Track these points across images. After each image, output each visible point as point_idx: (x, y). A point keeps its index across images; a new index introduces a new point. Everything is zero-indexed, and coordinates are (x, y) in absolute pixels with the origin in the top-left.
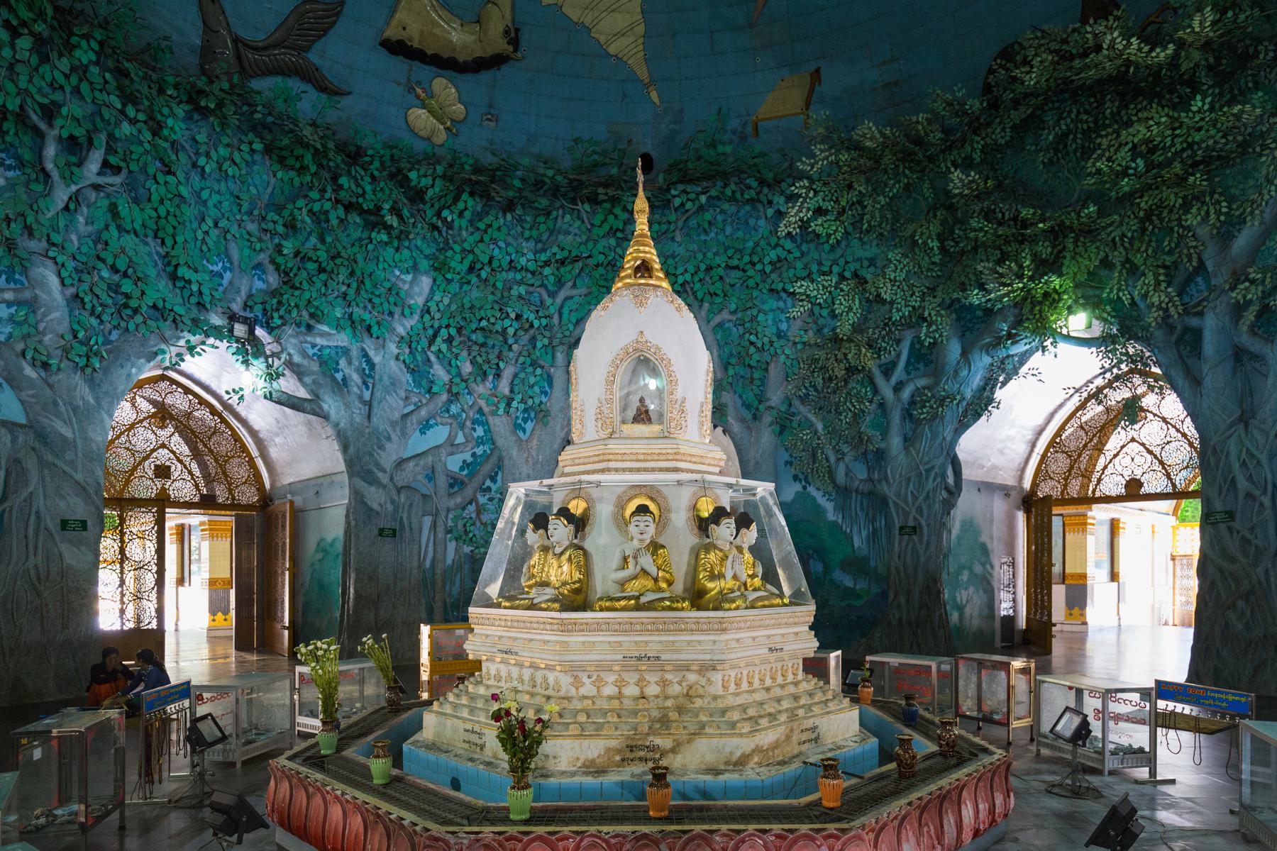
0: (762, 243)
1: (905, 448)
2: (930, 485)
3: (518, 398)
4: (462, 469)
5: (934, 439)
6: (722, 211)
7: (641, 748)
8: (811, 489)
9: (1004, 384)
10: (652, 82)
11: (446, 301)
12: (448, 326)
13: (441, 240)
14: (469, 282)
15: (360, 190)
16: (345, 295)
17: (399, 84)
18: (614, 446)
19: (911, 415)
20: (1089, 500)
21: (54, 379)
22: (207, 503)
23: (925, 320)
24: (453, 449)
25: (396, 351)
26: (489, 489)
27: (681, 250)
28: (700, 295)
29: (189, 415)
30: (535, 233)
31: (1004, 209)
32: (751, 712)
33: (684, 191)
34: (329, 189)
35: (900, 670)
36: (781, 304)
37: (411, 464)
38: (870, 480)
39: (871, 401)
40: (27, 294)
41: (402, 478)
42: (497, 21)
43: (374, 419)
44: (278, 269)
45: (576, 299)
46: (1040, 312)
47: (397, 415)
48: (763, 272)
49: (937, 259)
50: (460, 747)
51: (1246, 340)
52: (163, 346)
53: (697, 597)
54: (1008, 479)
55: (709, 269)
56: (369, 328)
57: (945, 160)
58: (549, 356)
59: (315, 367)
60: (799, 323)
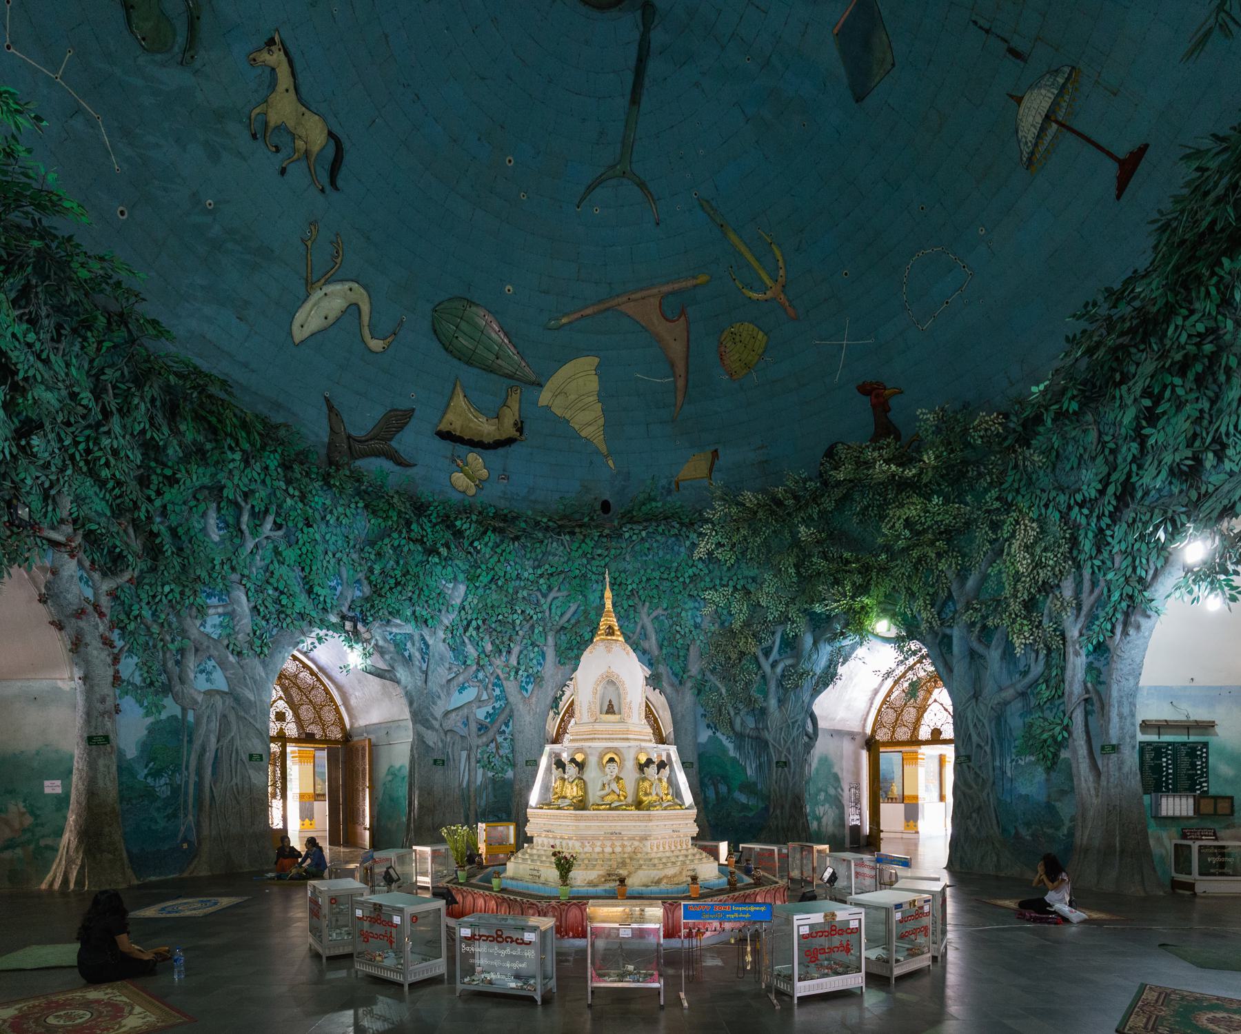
1: (779, 707)
2: (795, 733)
3: (523, 668)
4: (486, 718)
5: (797, 701)
6: (657, 541)
7: (613, 875)
8: (718, 734)
9: (843, 663)
10: (610, 454)
11: (476, 601)
12: (477, 619)
13: (472, 560)
14: (490, 588)
15: (425, 533)
18: (598, 727)
19: (782, 685)
20: (915, 742)
21: (243, 662)
22: (306, 738)
23: (789, 619)
24: (481, 704)
25: (443, 636)
26: (504, 732)
27: (630, 567)
29: (296, 676)
30: (533, 555)
31: (833, 551)
32: (664, 860)
33: (631, 529)
34: (404, 531)
35: (761, 853)
36: (697, 605)
37: (454, 714)
38: (757, 729)
39: (756, 674)
40: (229, 609)
41: (449, 724)
42: (510, 417)
43: (429, 684)
44: (370, 583)
45: (561, 599)
46: (859, 618)
47: (444, 681)
48: (684, 583)
49: (795, 580)
51: (975, 645)
52: (303, 638)
53: (639, 805)
54: (855, 726)
56: (426, 622)
57: (796, 517)
58: (543, 639)
59: (392, 648)
60: (709, 618)
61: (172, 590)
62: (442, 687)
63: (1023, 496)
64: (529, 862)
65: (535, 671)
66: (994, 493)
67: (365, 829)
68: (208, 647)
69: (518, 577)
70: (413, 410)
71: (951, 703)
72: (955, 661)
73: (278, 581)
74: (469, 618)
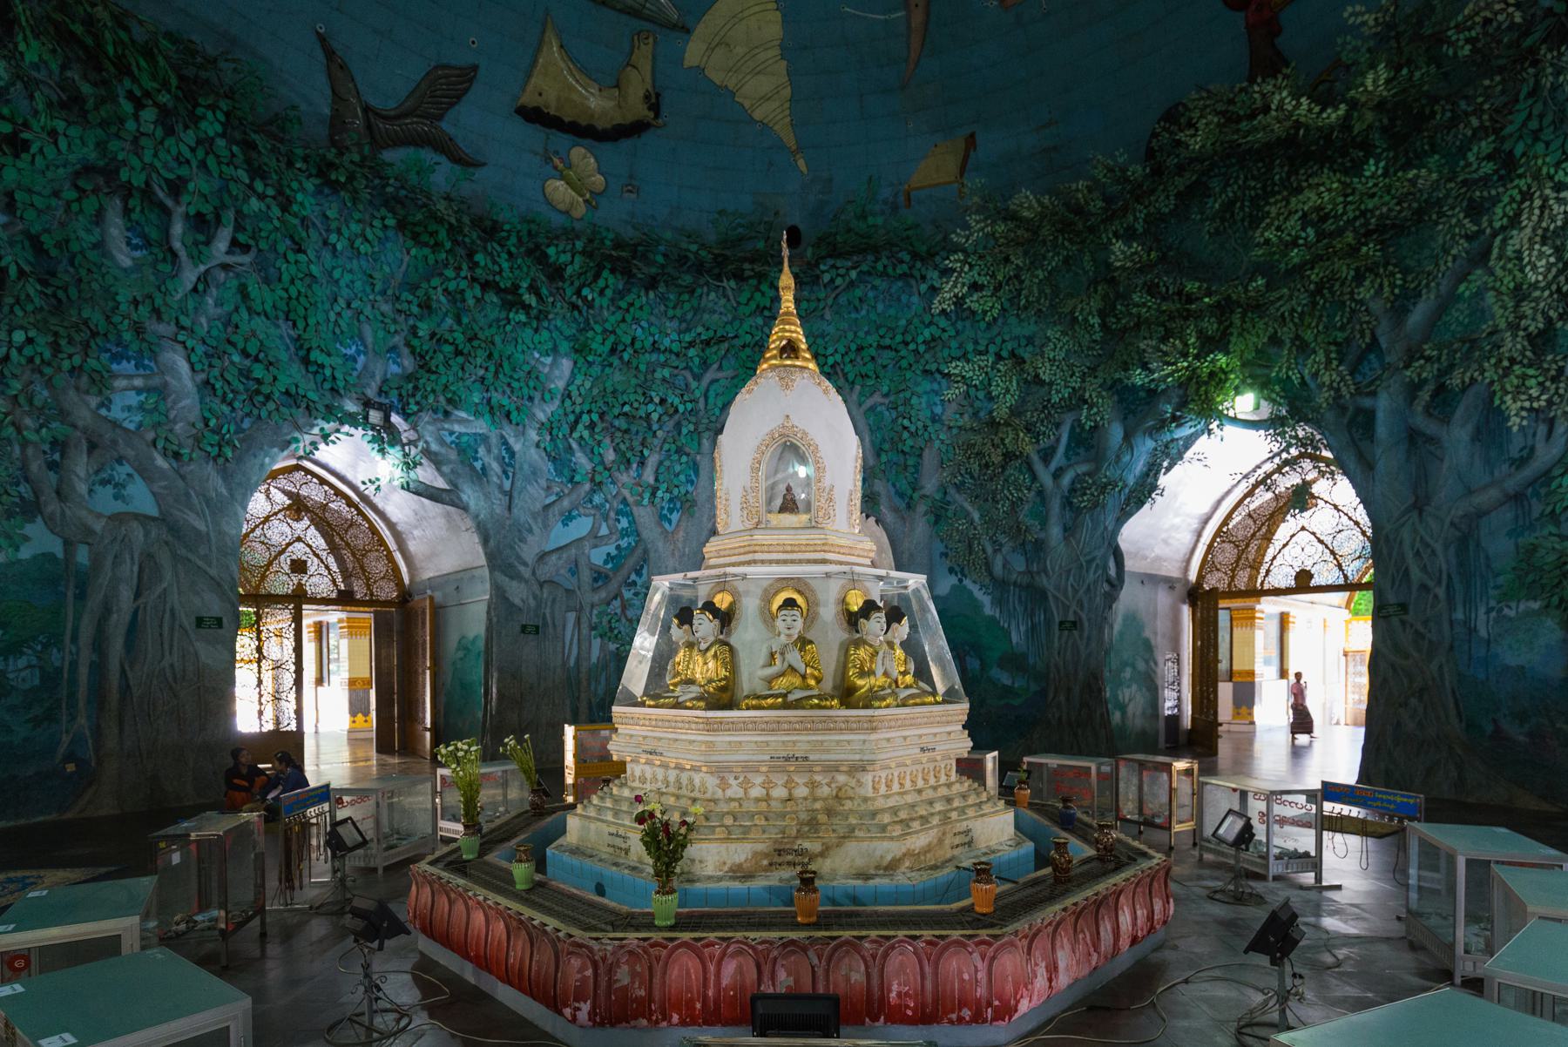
0: (916, 321)
1: (1065, 538)
2: (1091, 577)
3: (664, 487)
4: (606, 562)
6: (874, 288)
8: (967, 582)
11: (588, 385)
12: (589, 412)
13: (581, 320)
14: (611, 365)
16: (483, 379)
17: (536, 154)
18: (759, 537)
21: (186, 469)
22: (344, 599)
23: (1085, 402)
26: (634, 583)
27: (831, 329)
28: (851, 377)
30: (678, 312)
31: (1168, 282)
32: (903, 815)
33: (833, 266)
34: (465, 266)
36: (936, 386)
37: (554, 557)
38: (1029, 572)
39: (1029, 489)
40: (156, 381)
41: (545, 572)
42: (637, 85)
43: (515, 511)
45: (723, 382)
46: (1206, 392)
47: (538, 506)
48: (916, 351)
49: (1097, 337)
50: (605, 851)
51: (1420, 421)
52: (297, 434)
53: (847, 695)
55: (860, 349)
56: (508, 415)
57: (1106, 230)
59: (453, 455)
60: (954, 405)
61: (30, 341)
62: (535, 515)
63: (1547, 144)
64: (610, 817)
65: (683, 492)
66: (1485, 146)
67: (426, 729)
68: (114, 442)
69: (655, 347)
70: (475, 68)
71: (1369, 524)
72: (1379, 451)
73: (246, 340)
74: (578, 410)
